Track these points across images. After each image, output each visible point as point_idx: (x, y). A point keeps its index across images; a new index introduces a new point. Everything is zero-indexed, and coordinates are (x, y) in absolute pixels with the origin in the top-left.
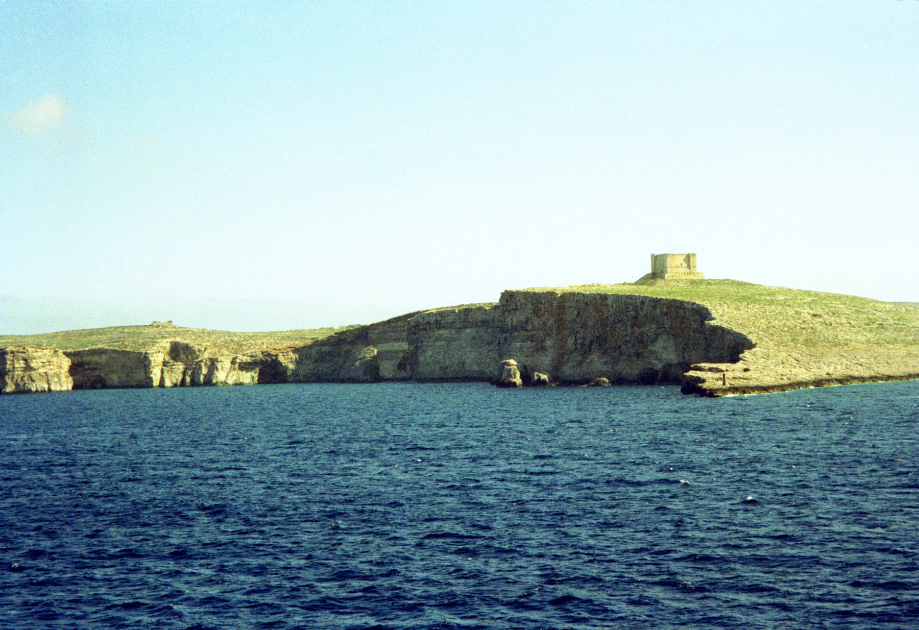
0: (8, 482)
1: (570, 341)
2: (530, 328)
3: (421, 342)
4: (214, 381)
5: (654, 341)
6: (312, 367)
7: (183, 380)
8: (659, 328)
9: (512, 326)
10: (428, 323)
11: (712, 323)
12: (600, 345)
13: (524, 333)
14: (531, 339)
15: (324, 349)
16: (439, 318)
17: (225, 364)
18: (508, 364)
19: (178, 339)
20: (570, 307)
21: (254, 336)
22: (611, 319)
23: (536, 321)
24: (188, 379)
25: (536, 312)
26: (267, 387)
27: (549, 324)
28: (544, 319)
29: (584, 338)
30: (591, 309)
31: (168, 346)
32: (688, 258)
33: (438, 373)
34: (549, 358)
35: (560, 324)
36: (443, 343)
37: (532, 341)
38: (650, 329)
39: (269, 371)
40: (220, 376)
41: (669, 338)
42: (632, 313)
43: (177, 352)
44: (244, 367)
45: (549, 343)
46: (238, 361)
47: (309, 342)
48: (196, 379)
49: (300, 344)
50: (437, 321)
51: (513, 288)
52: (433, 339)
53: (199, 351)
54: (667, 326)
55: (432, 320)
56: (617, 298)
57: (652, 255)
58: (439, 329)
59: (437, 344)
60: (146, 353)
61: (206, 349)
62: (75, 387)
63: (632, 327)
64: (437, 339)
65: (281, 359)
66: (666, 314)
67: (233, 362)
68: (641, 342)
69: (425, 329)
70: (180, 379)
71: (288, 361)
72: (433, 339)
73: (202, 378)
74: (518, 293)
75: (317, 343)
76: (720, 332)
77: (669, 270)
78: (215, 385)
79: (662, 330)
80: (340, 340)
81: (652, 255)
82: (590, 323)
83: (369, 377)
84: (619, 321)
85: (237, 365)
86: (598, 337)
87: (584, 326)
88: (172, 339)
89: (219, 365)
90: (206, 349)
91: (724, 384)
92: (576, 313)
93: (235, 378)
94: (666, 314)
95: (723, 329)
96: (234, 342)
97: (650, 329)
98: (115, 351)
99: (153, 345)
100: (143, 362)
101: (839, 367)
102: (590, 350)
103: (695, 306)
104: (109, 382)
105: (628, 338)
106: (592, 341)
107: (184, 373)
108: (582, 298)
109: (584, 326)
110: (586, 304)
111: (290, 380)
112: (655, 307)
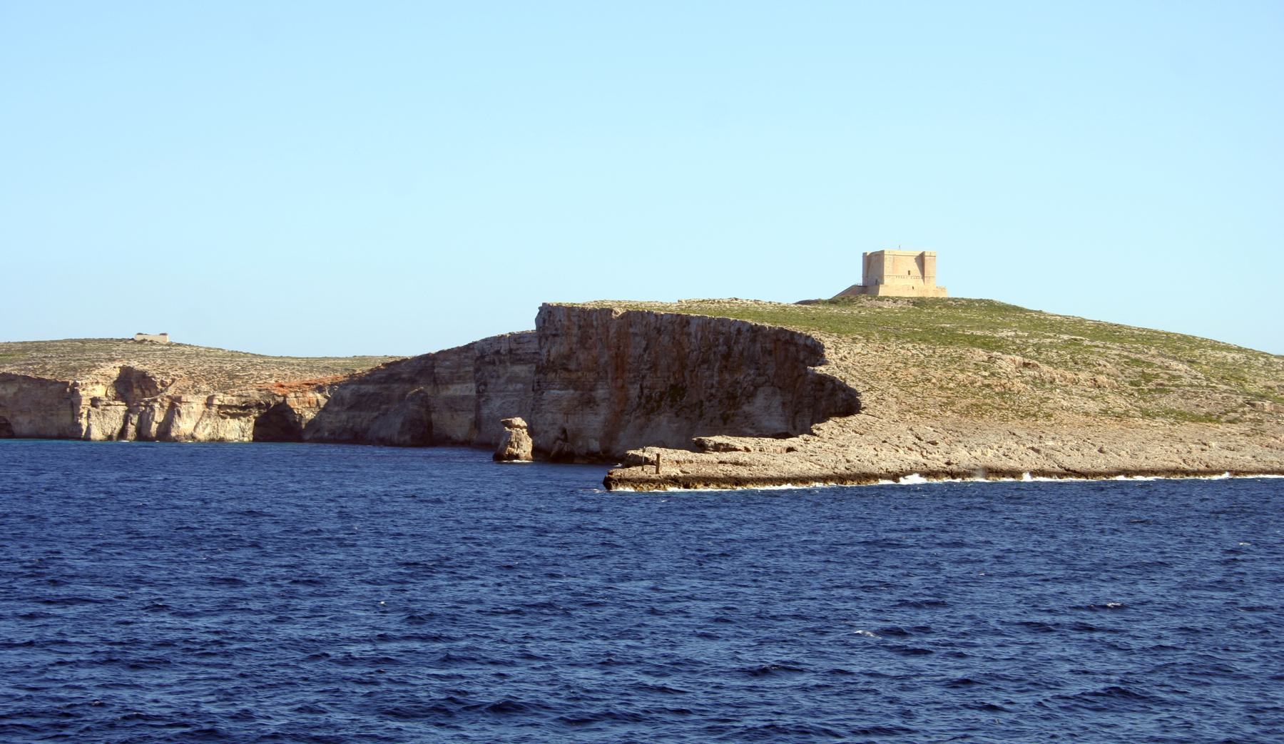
0: (594, 609)
1: (634, 391)
2: (573, 366)
3: (486, 385)
4: (173, 434)
5: (751, 396)
6: (344, 416)
7: (123, 433)
8: (759, 375)
9: (548, 361)
10: (498, 352)
11: (821, 370)
12: (673, 400)
13: (565, 375)
14: (569, 384)
15: (370, 388)
16: (514, 346)
17: (194, 405)
18: (511, 426)
19: (135, 364)
20: (635, 334)
21: (266, 361)
22: (694, 356)
23: (582, 356)
24: (131, 429)
25: (583, 341)
26: (264, 444)
27: (603, 360)
28: (595, 352)
29: (652, 388)
30: (665, 339)
31: (115, 373)
32: (921, 260)
33: (55, 433)
34: (601, 418)
35: (619, 364)
36: (520, 386)
37: (575, 389)
38: (746, 376)
39: (275, 423)
40: (183, 426)
41: (774, 394)
42: (723, 349)
43: (132, 386)
44: (227, 411)
45: (601, 393)
46: (216, 402)
47: (340, 377)
48: (144, 432)
49: (328, 378)
50: (511, 351)
51: (553, 300)
52: (502, 380)
53: (162, 383)
54: (771, 372)
55: (504, 348)
56: (705, 323)
57: (865, 254)
58: (513, 363)
59: (511, 388)
60: (75, 384)
61: (173, 380)
62: (254, 440)
63: (721, 371)
64: (510, 380)
65: (292, 401)
66: (770, 353)
67: (209, 404)
68: (732, 397)
69: (493, 363)
70: (119, 427)
71: (306, 406)
72: (502, 380)
73: (154, 427)
74: (559, 307)
75: (355, 380)
76: (829, 385)
77: (887, 280)
78: (175, 440)
79: (762, 379)
80: (391, 376)
81: (865, 254)
82: (663, 362)
83: (407, 437)
84: (704, 362)
85: (214, 410)
86: (672, 387)
87: (654, 367)
88: (125, 363)
89: (183, 409)
90: (173, 380)
91: (657, 472)
92: (644, 343)
93: (209, 430)
94: (770, 353)
95: (832, 380)
96: (222, 370)
97: (746, 376)
98: (26, 378)
99: (89, 372)
100: (68, 397)
101: (990, 453)
102: (659, 407)
103: (809, 342)
104: (17, 429)
105: (713, 391)
106: (662, 394)
107: (126, 420)
108: (652, 319)
109: (654, 367)
110: (659, 331)
111: (307, 437)
112: (754, 340)
